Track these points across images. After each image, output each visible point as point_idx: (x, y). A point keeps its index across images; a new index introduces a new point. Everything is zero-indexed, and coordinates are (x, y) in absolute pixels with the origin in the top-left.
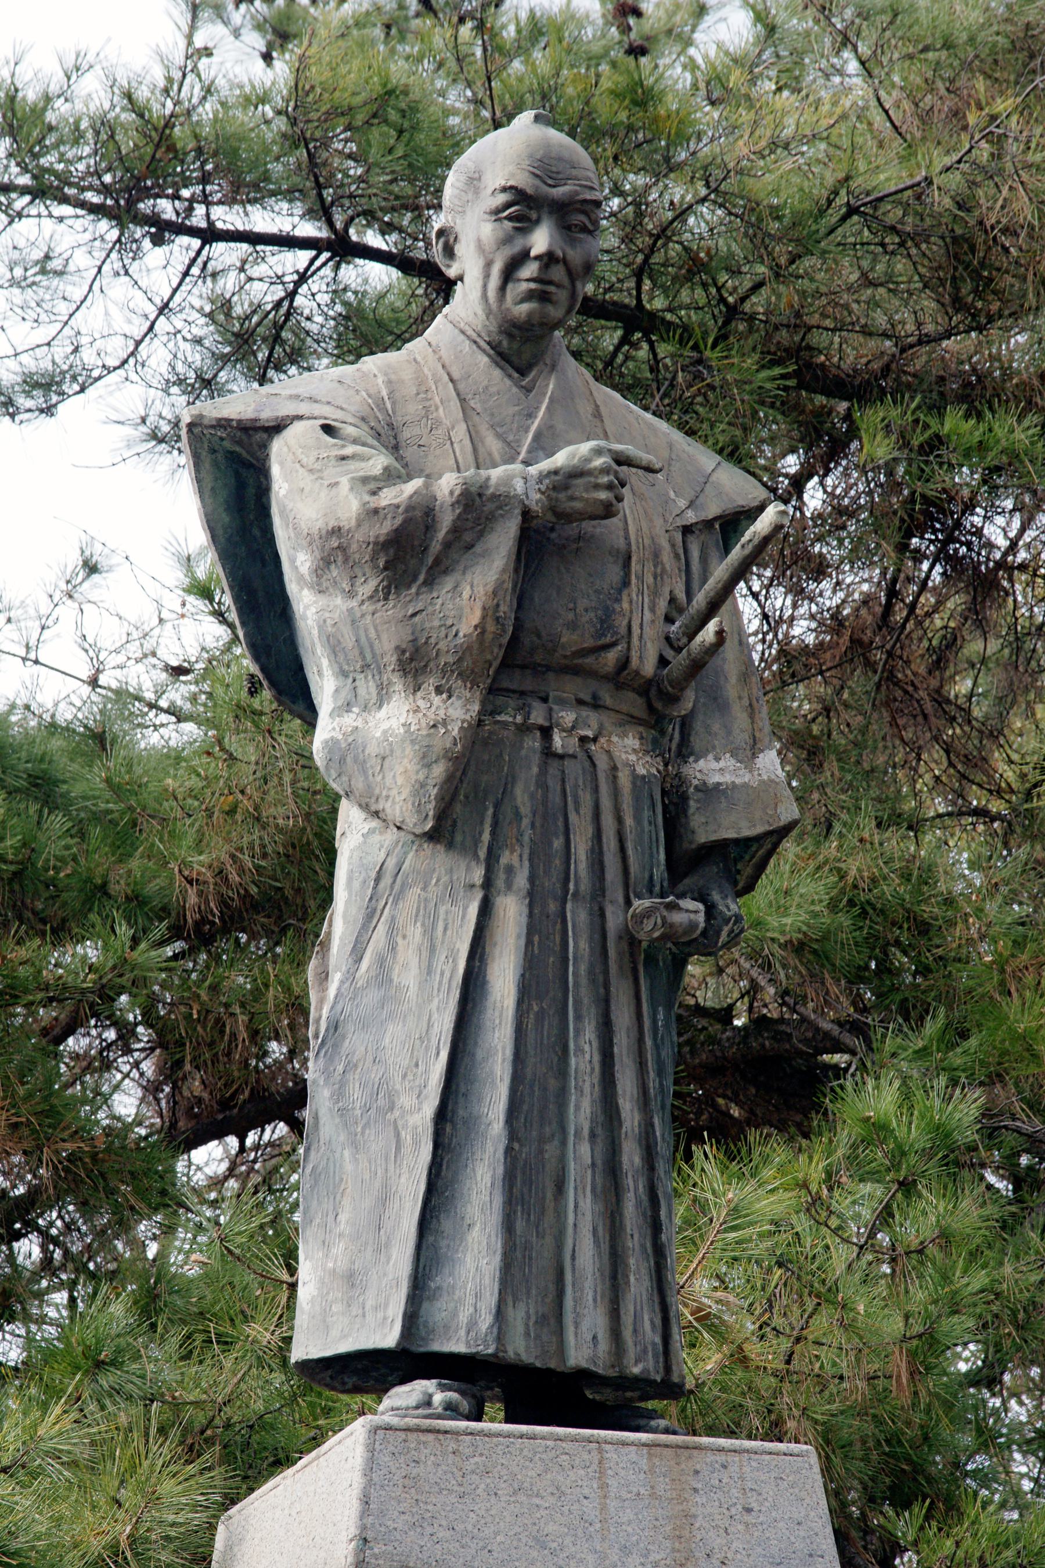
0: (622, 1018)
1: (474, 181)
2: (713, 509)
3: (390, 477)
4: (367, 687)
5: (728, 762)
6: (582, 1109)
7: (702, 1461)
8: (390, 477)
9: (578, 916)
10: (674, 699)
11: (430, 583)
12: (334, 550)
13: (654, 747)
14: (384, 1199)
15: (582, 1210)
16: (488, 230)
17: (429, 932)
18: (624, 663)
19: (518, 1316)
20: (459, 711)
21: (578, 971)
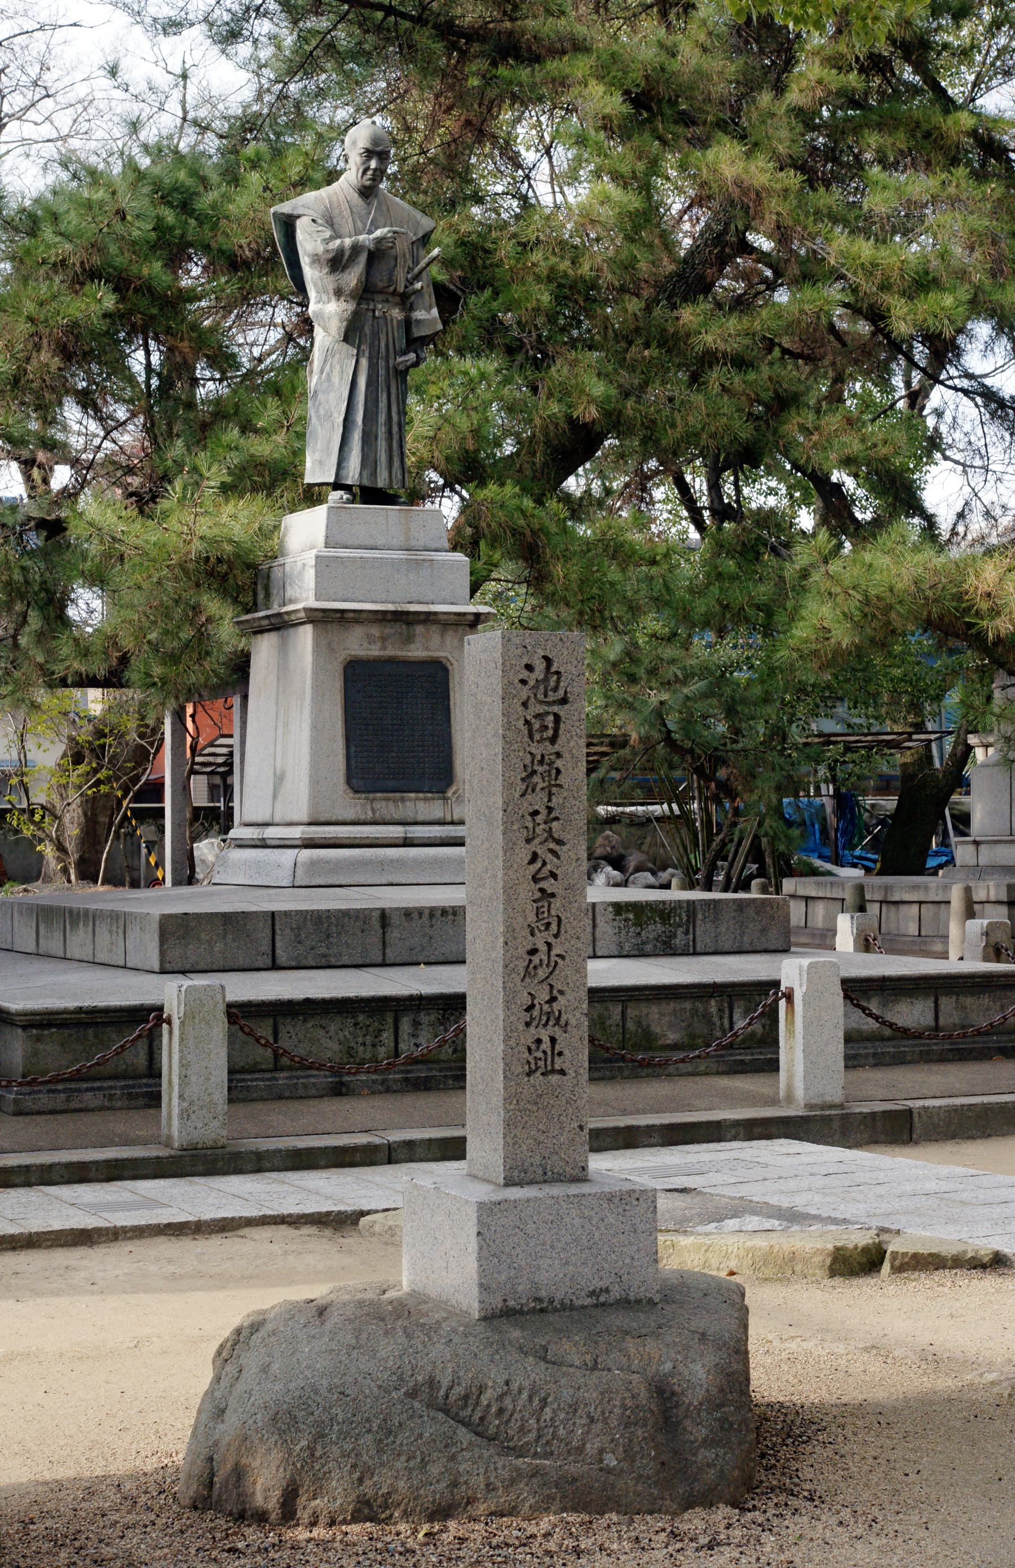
0: (393, 390)
1: (354, 143)
2: (420, 234)
3: (332, 238)
4: (324, 297)
5: (423, 312)
6: (382, 418)
7: (413, 514)
8: (332, 238)
9: (382, 363)
10: (409, 298)
11: (343, 271)
12: (316, 259)
13: (403, 310)
14: (330, 441)
15: (382, 445)
16: (358, 160)
17: (341, 367)
18: (395, 290)
19: (365, 473)
20: (351, 307)
21: (381, 379)
